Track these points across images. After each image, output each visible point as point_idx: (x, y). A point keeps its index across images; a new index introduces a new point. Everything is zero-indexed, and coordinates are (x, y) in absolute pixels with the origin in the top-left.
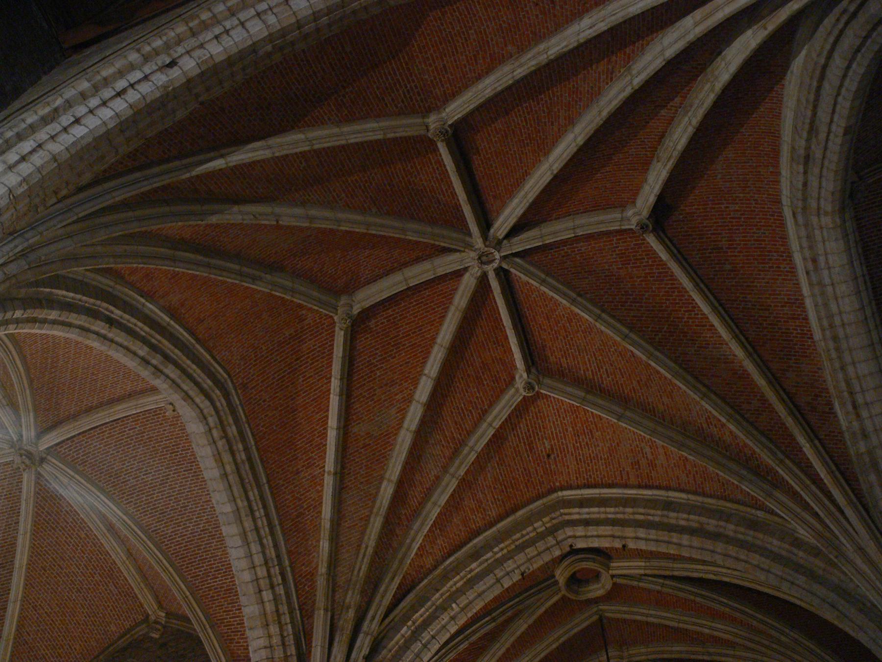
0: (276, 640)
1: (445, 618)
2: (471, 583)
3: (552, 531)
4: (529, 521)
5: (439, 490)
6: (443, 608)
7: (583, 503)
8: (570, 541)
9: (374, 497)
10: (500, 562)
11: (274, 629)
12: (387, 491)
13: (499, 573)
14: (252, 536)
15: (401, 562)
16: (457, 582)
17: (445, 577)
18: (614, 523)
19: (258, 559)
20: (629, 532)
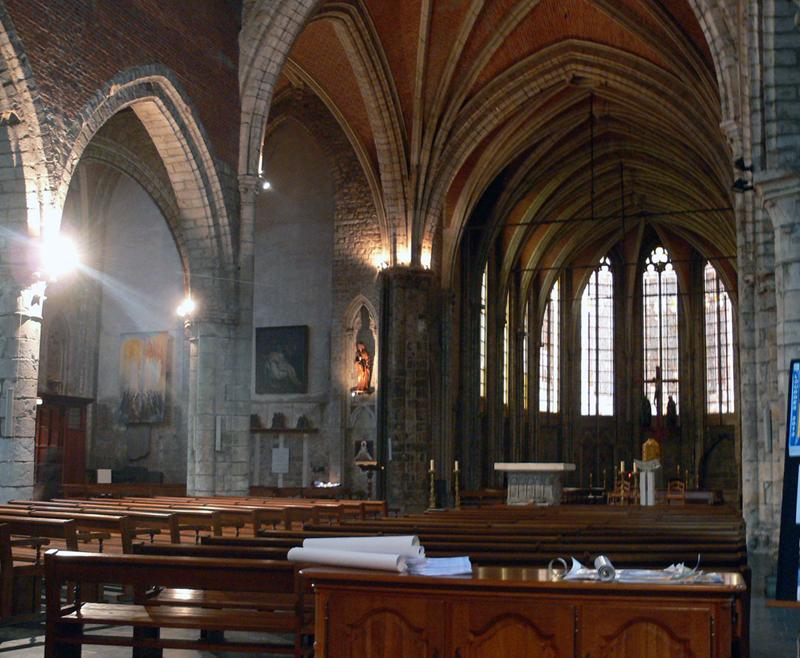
0: (392, 139)
1: (491, 116)
2: (509, 94)
3: (563, 65)
4: (549, 56)
5: (491, 43)
6: (491, 110)
7: (584, 50)
8: (574, 72)
9: (450, 50)
10: (528, 82)
11: (390, 133)
12: (458, 49)
13: (526, 89)
14: (375, 82)
15: (467, 85)
16: (500, 93)
17: (492, 90)
18: (602, 67)
19: (379, 95)
20: (611, 76)
